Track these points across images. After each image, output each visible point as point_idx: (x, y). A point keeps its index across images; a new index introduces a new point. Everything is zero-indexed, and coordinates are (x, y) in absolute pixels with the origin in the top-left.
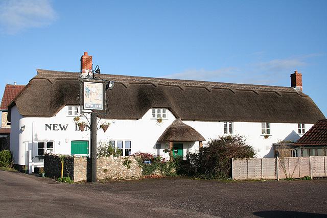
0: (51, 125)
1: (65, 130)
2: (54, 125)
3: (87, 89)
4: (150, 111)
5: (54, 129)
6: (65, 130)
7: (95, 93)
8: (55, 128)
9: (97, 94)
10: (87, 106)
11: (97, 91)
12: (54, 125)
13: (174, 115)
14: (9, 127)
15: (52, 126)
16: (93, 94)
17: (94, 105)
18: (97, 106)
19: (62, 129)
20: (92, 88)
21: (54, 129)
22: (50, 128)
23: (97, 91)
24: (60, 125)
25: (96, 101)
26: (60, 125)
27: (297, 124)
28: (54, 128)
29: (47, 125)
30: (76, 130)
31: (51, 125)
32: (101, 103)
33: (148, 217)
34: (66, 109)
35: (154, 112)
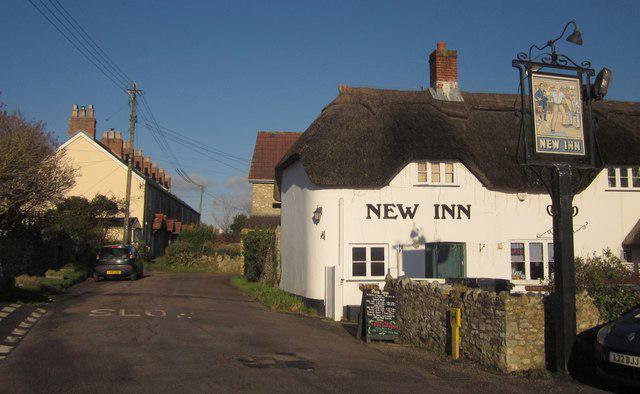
0: (379, 205)
1: (412, 216)
2: (386, 206)
3: (540, 94)
4: (604, 173)
5: (386, 217)
6: (412, 216)
7: (561, 107)
8: (390, 214)
9: (567, 109)
10: (542, 143)
11: (568, 102)
12: (386, 206)
13: (192, 210)
14: (629, 266)
15: (382, 208)
16: (556, 109)
17: (561, 141)
18: (570, 145)
19: (404, 216)
20: (554, 94)
21: (386, 217)
22: (378, 213)
23: (568, 102)
24: (400, 206)
25: (563, 129)
26: (400, 206)
27: (546, 200)
28: (386, 214)
29: (370, 207)
30: (437, 217)
31: (379, 205)
32: (580, 135)
33: (530, 392)
34: (412, 169)
35: (612, 173)
